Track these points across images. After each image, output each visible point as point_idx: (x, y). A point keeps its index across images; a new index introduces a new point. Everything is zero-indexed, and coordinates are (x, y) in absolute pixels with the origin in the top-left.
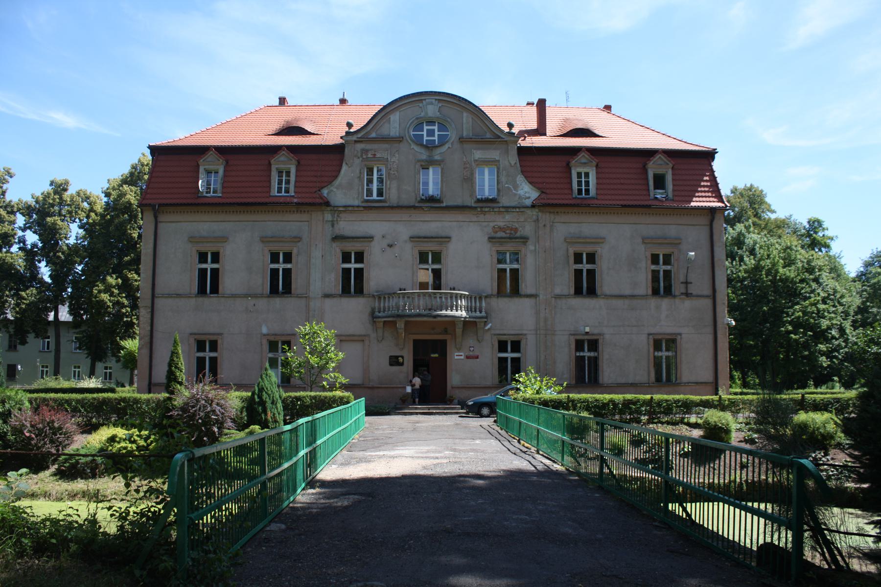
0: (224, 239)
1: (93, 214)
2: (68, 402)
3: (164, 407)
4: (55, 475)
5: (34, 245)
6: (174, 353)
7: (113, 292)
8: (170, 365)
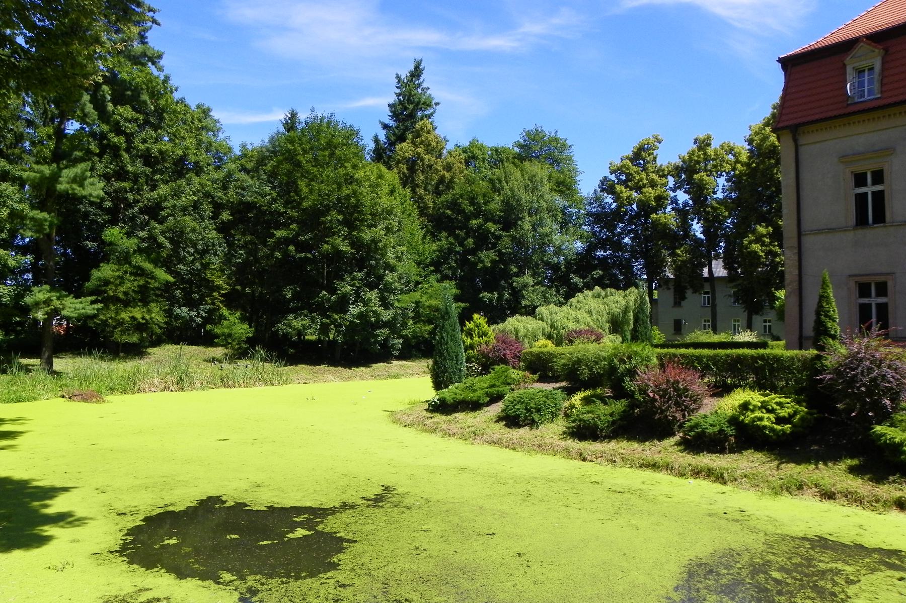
0: (889, 151)
1: (739, 166)
2: (699, 358)
3: (813, 367)
4: (678, 444)
5: (686, 204)
6: (823, 298)
7: (764, 242)
8: (818, 314)
